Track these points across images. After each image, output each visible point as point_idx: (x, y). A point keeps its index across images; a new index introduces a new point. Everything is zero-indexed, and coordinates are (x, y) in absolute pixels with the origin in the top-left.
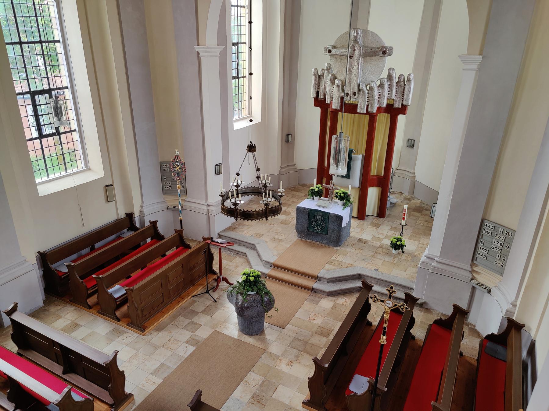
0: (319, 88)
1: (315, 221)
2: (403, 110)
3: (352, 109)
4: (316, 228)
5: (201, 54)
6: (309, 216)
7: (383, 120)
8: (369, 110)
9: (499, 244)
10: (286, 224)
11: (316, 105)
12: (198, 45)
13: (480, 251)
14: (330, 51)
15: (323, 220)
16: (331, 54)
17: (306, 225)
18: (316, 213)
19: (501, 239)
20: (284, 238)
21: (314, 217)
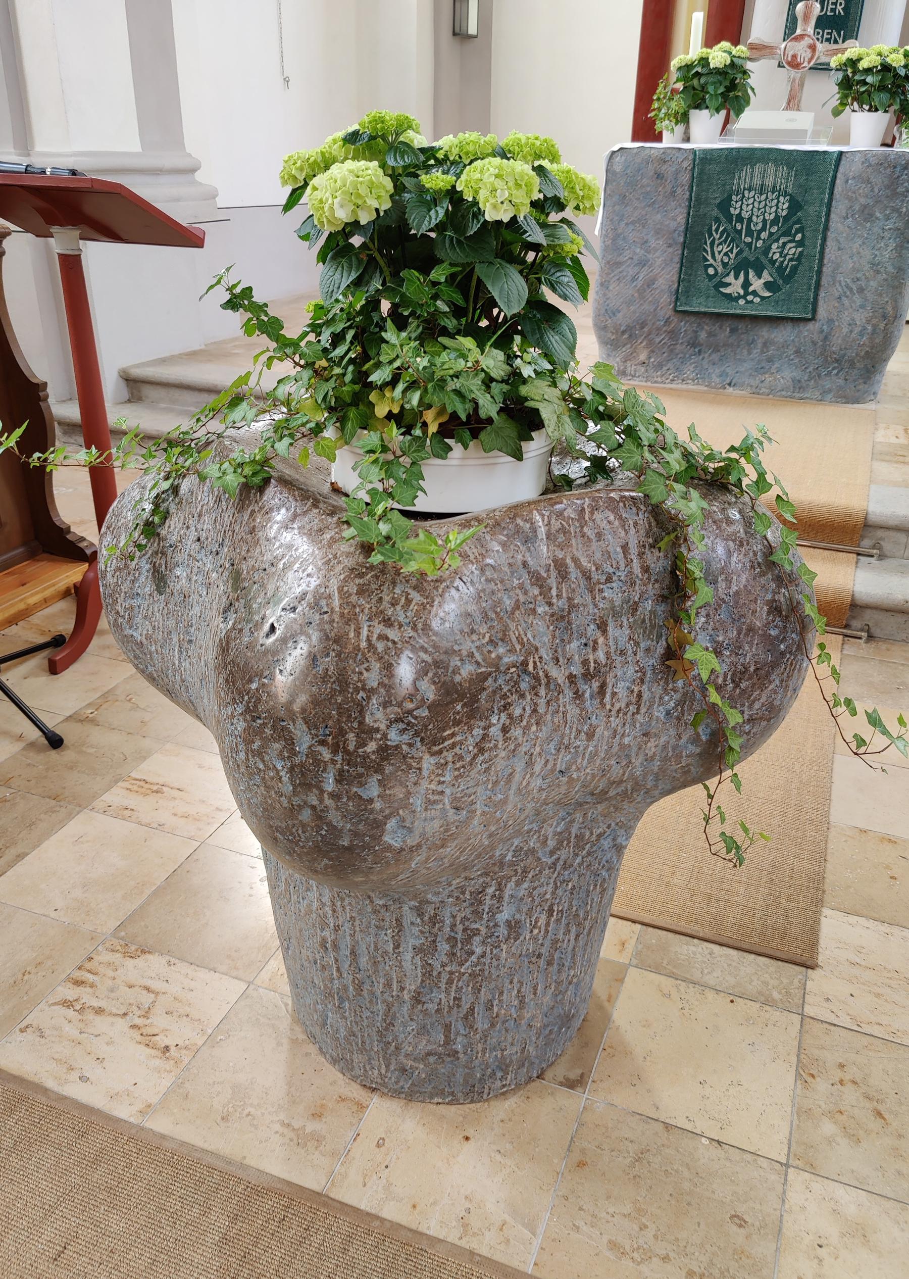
1: (732, 237)
6: (696, 203)
17: (666, 276)
21: (724, 206)
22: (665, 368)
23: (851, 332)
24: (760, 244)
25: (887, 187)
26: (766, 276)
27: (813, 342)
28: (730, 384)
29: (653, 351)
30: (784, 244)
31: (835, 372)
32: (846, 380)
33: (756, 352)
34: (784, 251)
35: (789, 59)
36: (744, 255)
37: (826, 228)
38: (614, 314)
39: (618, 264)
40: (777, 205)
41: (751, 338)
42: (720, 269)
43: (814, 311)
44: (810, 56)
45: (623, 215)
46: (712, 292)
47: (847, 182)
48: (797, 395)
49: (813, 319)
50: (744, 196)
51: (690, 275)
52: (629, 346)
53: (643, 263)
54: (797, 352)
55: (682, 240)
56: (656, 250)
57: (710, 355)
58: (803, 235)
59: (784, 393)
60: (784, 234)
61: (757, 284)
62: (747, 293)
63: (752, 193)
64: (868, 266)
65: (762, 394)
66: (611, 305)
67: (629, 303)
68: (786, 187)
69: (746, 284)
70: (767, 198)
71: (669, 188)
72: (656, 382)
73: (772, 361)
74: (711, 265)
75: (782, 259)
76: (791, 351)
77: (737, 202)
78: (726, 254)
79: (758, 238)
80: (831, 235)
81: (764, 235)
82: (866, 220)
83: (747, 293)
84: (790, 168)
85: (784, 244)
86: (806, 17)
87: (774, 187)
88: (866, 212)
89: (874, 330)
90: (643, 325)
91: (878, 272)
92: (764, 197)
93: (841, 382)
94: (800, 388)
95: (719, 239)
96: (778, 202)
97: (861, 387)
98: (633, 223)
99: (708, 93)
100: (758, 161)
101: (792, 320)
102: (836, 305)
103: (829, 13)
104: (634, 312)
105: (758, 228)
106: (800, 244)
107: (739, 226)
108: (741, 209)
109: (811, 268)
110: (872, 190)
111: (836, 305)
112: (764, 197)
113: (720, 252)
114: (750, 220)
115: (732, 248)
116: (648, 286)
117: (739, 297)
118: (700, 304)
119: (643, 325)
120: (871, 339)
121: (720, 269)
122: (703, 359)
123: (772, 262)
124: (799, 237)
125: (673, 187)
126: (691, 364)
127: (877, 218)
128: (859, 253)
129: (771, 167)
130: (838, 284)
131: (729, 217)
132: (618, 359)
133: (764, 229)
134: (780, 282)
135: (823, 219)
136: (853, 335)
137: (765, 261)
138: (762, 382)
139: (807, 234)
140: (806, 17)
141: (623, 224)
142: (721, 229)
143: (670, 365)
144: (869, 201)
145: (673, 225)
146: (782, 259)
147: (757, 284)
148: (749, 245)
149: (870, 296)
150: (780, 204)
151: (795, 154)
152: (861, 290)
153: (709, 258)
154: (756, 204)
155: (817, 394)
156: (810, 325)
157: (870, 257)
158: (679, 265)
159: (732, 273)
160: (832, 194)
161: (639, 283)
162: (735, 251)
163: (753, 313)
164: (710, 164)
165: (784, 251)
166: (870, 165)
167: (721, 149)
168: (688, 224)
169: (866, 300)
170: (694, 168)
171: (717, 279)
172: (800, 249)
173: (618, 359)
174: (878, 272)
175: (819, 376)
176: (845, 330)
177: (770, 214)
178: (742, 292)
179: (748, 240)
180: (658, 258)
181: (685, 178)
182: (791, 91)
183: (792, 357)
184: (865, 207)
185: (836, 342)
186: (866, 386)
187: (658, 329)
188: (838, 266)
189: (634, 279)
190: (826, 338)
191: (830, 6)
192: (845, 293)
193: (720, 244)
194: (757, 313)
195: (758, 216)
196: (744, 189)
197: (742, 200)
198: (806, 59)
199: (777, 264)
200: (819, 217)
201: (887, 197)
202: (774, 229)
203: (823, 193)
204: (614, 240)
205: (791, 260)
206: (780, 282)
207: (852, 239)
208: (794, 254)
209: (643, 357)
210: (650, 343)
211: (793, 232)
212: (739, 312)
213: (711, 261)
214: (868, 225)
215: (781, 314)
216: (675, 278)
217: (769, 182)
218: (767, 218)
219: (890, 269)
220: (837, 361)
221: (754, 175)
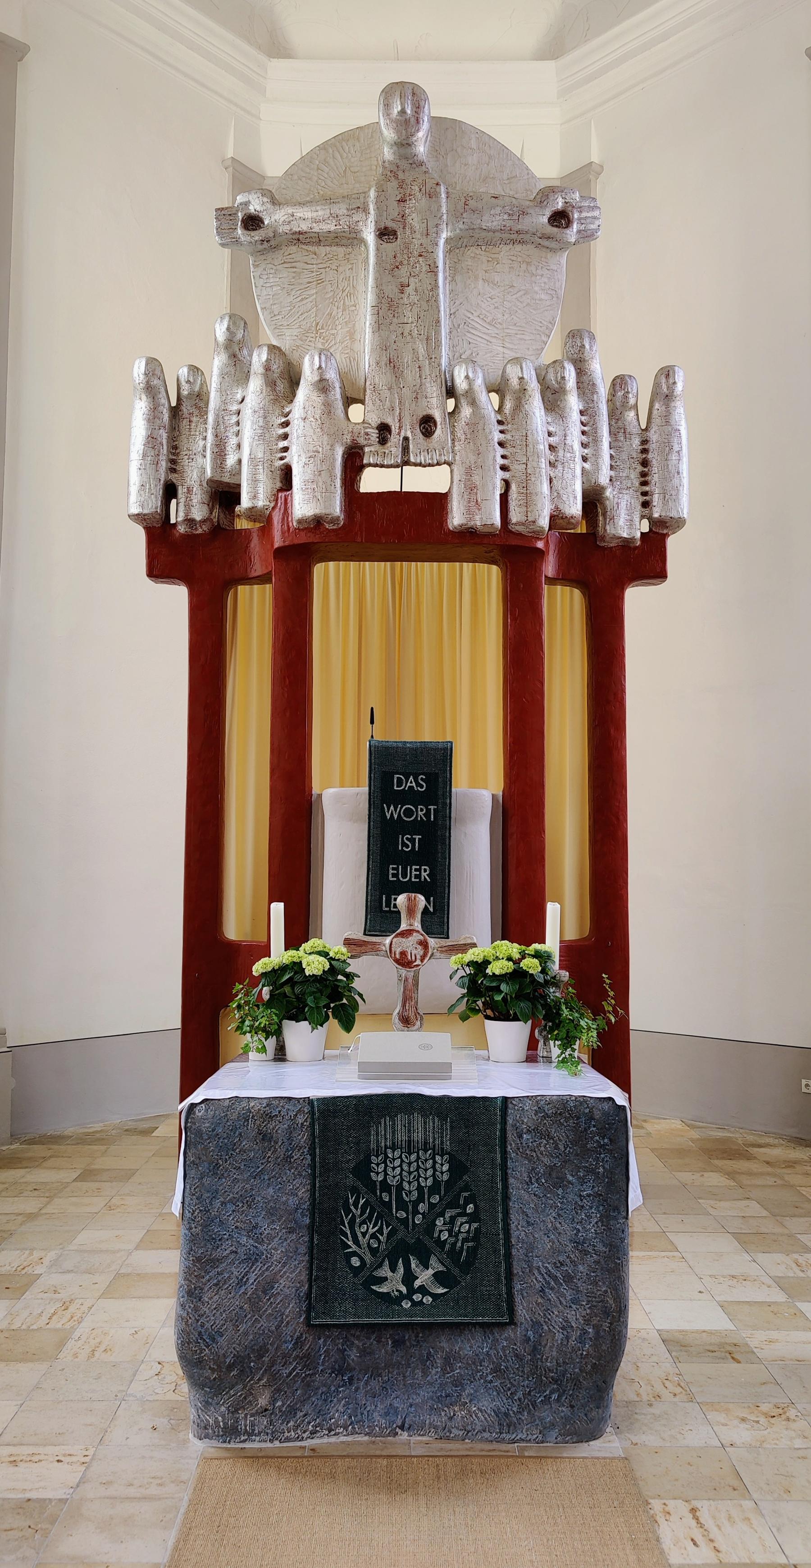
0: (174, 466)
1: (380, 1212)
2: (647, 559)
3: (404, 528)
4: (392, 1282)
6: (322, 1172)
7: (563, 611)
8: (515, 516)
10: (28, 1357)
15: (454, 1191)
16: (257, 235)
17: (290, 1277)
18: (382, 1133)
20: (69, 1474)
21: (363, 1170)
22: (300, 1414)
23: (568, 1338)
24: (418, 1220)
25: (574, 1143)
26: (436, 1265)
27: (517, 1356)
28: (402, 1428)
29: (278, 1390)
30: (453, 1219)
31: (555, 1396)
32: (572, 1407)
33: (434, 1373)
34: (454, 1228)
35: (398, 956)
36: (400, 1235)
37: (506, 1197)
38: (213, 1340)
39: (214, 1262)
40: (434, 1167)
41: (425, 1353)
42: (368, 1258)
43: (511, 1311)
44: (422, 953)
45: (217, 1191)
46: (361, 1292)
47: (520, 1137)
48: (507, 1437)
49: (512, 1322)
50: (386, 1157)
51: (326, 1269)
52: (241, 1386)
53: (252, 1258)
54: (497, 1370)
55: (308, 1221)
56: (271, 1238)
57: (367, 1383)
58: (476, 1206)
59: (486, 1435)
60: (450, 1206)
61: (424, 1277)
62: (411, 1291)
63: (397, 1153)
64: (570, 1246)
65: (453, 1439)
66: (208, 1325)
67: (236, 1321)
68: (442, 1143)
69: (409, 1278)
70: (418, 1158)
71: (281, 1152)
72: (288, 1440)
73: (462, 1385)
74: (354, 1254)
75: (453, 1240)
76: (487, 1368)
77: (378, 1165)
78: (373, 1236)
79: (416, 1212)
80: (514, 1205)
81: (422, 1207)
82: (556, 1186)
83: (411, 1291)
84: (443, 1119)
85: (453, 1219)
86: (411, 912)
87: (426, 1143)
88: (554, 1175)
89: (597, 1333)
90: (261, 1352)
91: (586, 1253)
92: (413, 1157)
93: (565, 1410)
94: (509, 1426)
95: (361, 1215)
96: (435, 1162)
97: (594, 1413)
98: (233, 1201)
99: (307, 1005)
100: (400, 1110)
101: (483, 1325)
102: (540, 1300)
103: (413, 880)
104: (246, 1334)
105: (414, 1198)
106: (474, 1218)
107: (386, 1197)
108: (386, 1174)
109: (496, 1251)
110: (556, 1147)
111: (540, 1300)
112: (413, 1157)
113: (364, 1234)
114: (400, 1188)
115: (381, 1228)
116: (265, 1292)
117: (402, 1297)
118: (345, 1312)
119: (261, 1352)
120: (596, 1346)
121: (368, 1258)
122: (357, 1389)
123: (441, 1244)
124: (470, 1208)
125: (287, 1150)
126: (339, 1401)
127: (570, 1182)
128: (556, 1228)
129: (418, 1120)
130: (536, 1272)
131: (371, 1185)
132: (223, 1409)
133: (421, 1199)
134: (456, 1271)
135: (500, 1186)
136: (572, 1343)
137: (427, 1240)
138: (451, 1418)
139: (482, 1205)
140: (411, 912)
141: (217, 1204)
142: (362, 1202)
143: (307, 1408)
144: (556, 1161)
145: (292, 1201)
146: (453, 1240)
147: (424, 1277)
148: (404, 1222)
149: (583, 1287)
150: (438, 1166)
151: (446, 1101)
152: (569, 1279)
153: (350, 1243)
154: (405, 1167)
155: (536, 1434)
156: (509, 1332)
157: (571, 1233)
158: (307, 1258)
159: (387, 1262)
160: (504, 1153)
161: (250, 1288)
162: (385, 1231)
163: (425, 1320)
164: (335, 1117)
165: (454, 1228)
166: (547, 1116)
167: (347, 1097)
168: (314, 1200)
169: (578, 1292)
170: (312, 1125)
171: (365, 1273)
172: (475, 1225)
173: (223, 1409)
174: (586, 1253)
175: (534, 1405)
176: (559, 1336)
177: (426, 1179)
178: (404, 1289)
179: (402, 1214)
180: (276, 1249)
181: (302, 1138)
182: (404, 992)
183: (490, 1378)
184: (552, 1168)
185: (551, 1354)
186: (600, 1411)
187: (285, 1356)
188: (531, 1248)
189: (241, 1282)
190: (535, 1349)
191: (414, 873)
192: (549, 1283)
193: (363, 1222)
194: (431, 1320)
195: (409, 1183)
196: (386, 1147)
197: (385, 1162)
198: (418, 957)
199: (447, 1246)
200: (493, 1181)
201: (577, 1155)
202: (435, 1199)
203: (492, 1151)
204: (205, 1226)
205: (465, 1240)
206: (456, 1271)
207: (543, 1211)
208: (468, 1232)
209: (263, 1401)
210: (274, 1377)
211: (461, 1202)
212: (405, 1319)
213: (354, 1248)
214: (560, 1191)
215: (467, 1320)
216: (304, 1277)
217: (418, 1136)
218: (423, 1184)
219: (600, 1247)
220: (555, 1381)
221: (399, 1128)
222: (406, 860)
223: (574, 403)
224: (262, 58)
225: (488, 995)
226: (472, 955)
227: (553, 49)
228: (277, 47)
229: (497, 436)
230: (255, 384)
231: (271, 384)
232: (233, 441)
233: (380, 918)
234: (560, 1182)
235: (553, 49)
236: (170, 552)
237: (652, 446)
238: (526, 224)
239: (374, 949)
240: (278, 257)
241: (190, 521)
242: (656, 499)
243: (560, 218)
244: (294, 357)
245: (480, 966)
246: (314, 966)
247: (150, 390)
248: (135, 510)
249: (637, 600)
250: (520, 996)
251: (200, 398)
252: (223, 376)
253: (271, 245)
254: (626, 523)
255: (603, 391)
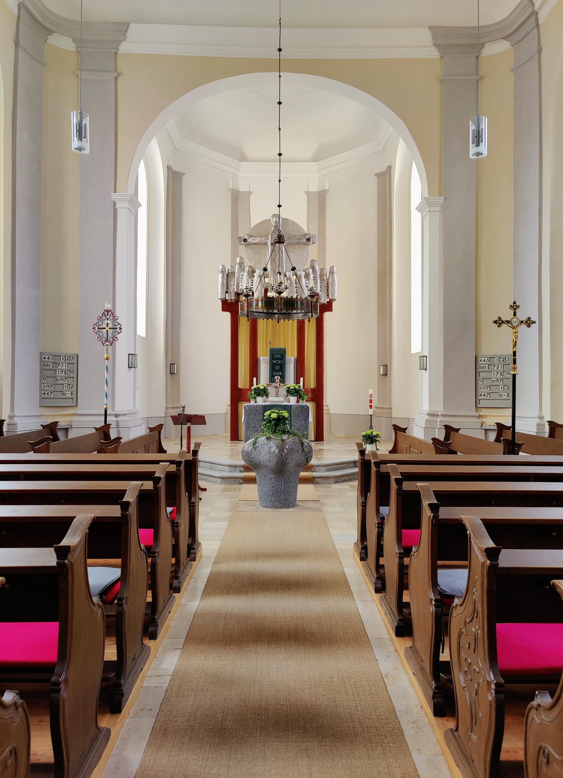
2: (328, 307)
5: (117, 204)
9: (499, 374)
11: (224, 309)
12: (115, 192)
13: (482, 390)
14: (245, 240)
16: (246, 243)
19: (500, 368)
53: (255, 427)
222: (277, 371)
223: (312, 276)
224: (240, 162)
225: (290, 392)
226: (288, 386)
227: (316, 159)
228: (243, 158)
229: (295, 286)
230: (245, 274)
231: (249, 274)
232: (241, 284)
233: (272, 380)
234: (299, 416)
235: (316, 159)
236: (227, 306)
237: (329, 283)
238: (301, 241)
239: (271, 385)
240: (250, 247)
241: (231, 300)
242: (330, 295)
243: (308, 240)
244: (254, 268)
245: (289, 388)
246: (262, 388)
247: (223, 272)
248: (220, 298)
249: (327, 315)
250: (295, 392)
251: (233, 273)
252: (238, 270)
253: (249, 244)
254: (324, 300)
255: (318, 272)
